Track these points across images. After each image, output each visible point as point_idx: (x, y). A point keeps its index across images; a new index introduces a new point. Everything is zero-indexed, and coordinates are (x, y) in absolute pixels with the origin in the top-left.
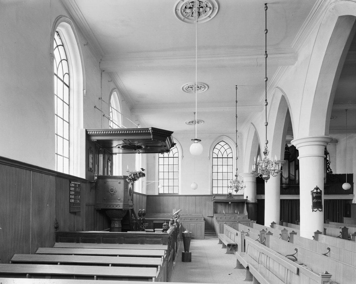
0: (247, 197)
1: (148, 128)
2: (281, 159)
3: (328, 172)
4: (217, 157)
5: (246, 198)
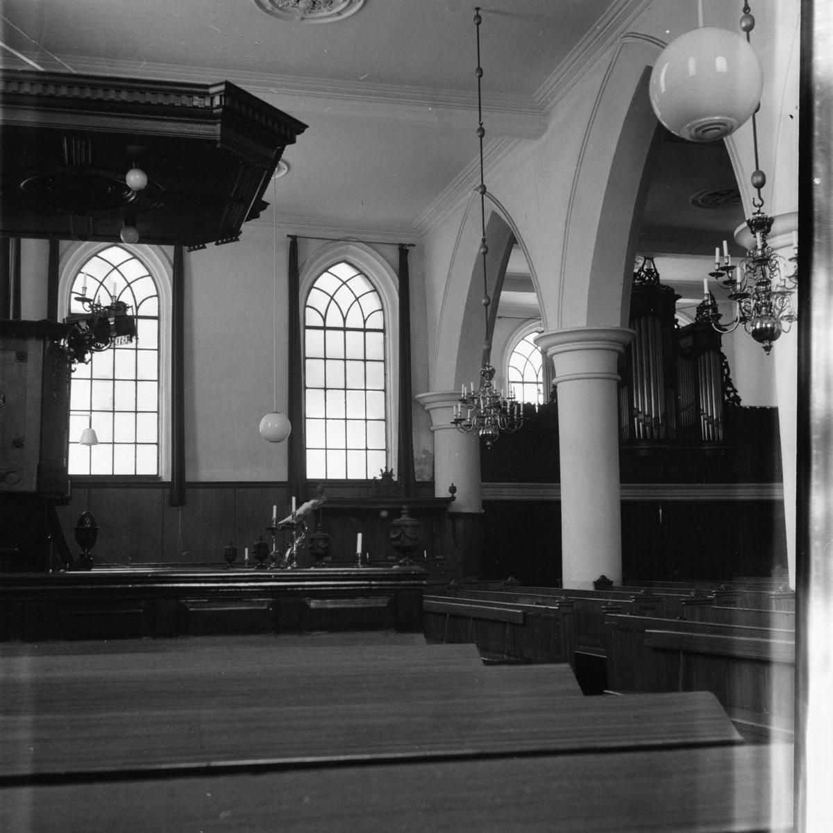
0: (453, 489)
1: (207, 87)
2: (622, 325)
3: (726, 398)
4: (321, 324)
5: (450, 495)
